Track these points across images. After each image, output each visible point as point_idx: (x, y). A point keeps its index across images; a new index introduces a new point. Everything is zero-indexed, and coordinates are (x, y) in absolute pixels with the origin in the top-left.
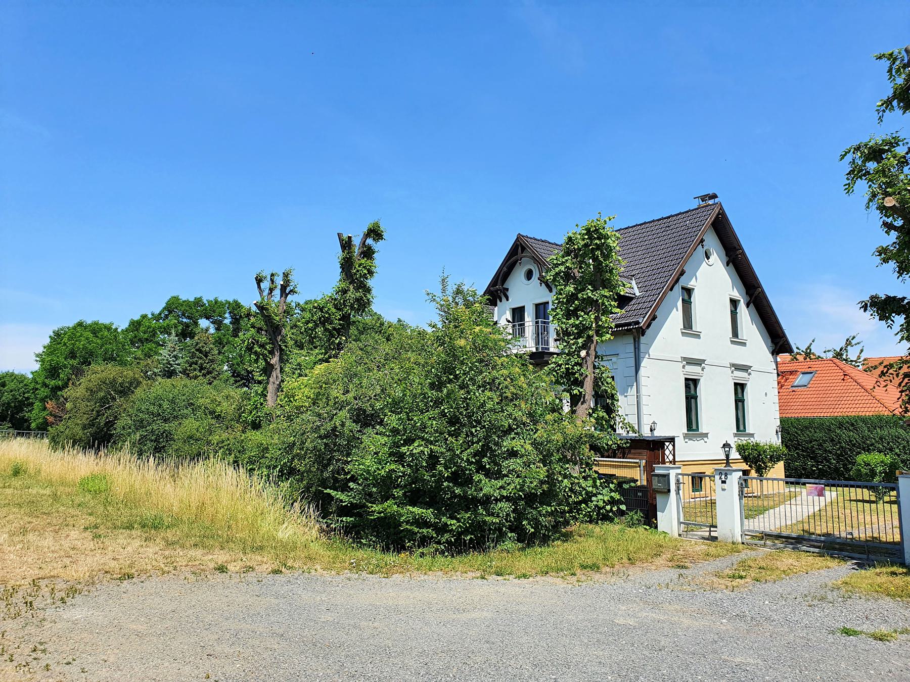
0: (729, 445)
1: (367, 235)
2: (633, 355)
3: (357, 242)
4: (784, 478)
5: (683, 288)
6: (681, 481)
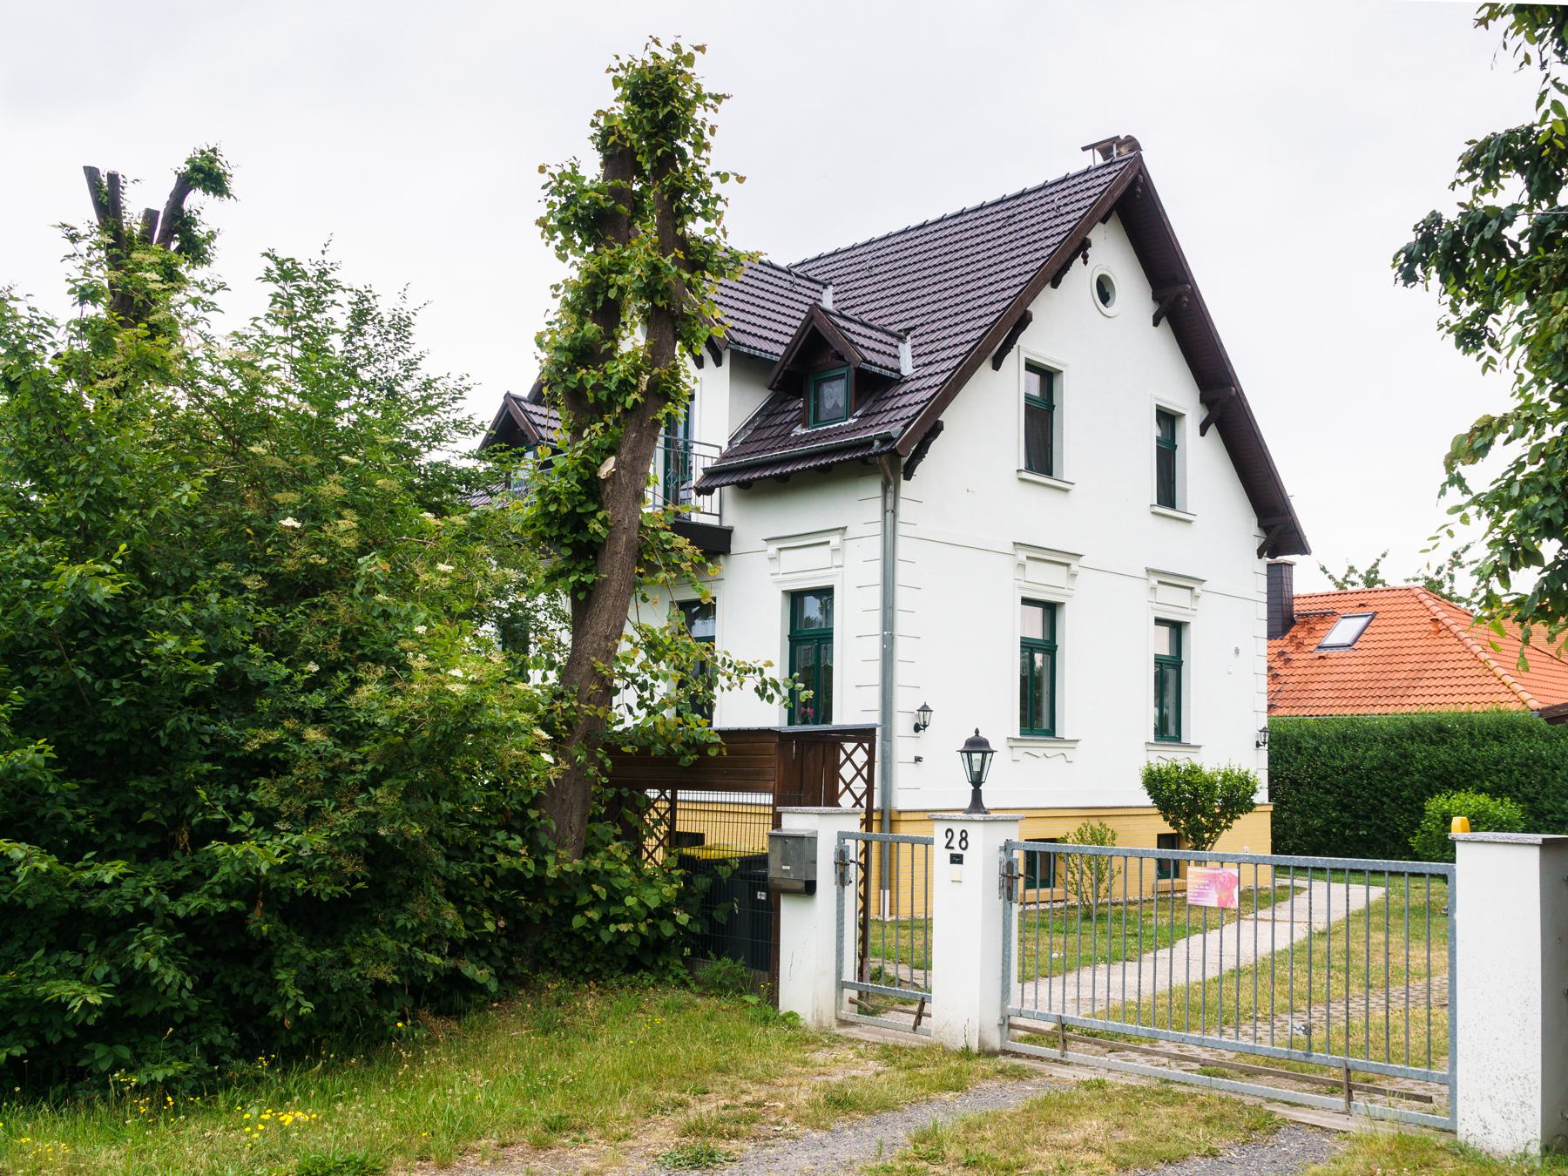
0: (985, 743)
1: (185, 184)
2: (878, 529)
4: (1269, 854)
5: (1031, 367)
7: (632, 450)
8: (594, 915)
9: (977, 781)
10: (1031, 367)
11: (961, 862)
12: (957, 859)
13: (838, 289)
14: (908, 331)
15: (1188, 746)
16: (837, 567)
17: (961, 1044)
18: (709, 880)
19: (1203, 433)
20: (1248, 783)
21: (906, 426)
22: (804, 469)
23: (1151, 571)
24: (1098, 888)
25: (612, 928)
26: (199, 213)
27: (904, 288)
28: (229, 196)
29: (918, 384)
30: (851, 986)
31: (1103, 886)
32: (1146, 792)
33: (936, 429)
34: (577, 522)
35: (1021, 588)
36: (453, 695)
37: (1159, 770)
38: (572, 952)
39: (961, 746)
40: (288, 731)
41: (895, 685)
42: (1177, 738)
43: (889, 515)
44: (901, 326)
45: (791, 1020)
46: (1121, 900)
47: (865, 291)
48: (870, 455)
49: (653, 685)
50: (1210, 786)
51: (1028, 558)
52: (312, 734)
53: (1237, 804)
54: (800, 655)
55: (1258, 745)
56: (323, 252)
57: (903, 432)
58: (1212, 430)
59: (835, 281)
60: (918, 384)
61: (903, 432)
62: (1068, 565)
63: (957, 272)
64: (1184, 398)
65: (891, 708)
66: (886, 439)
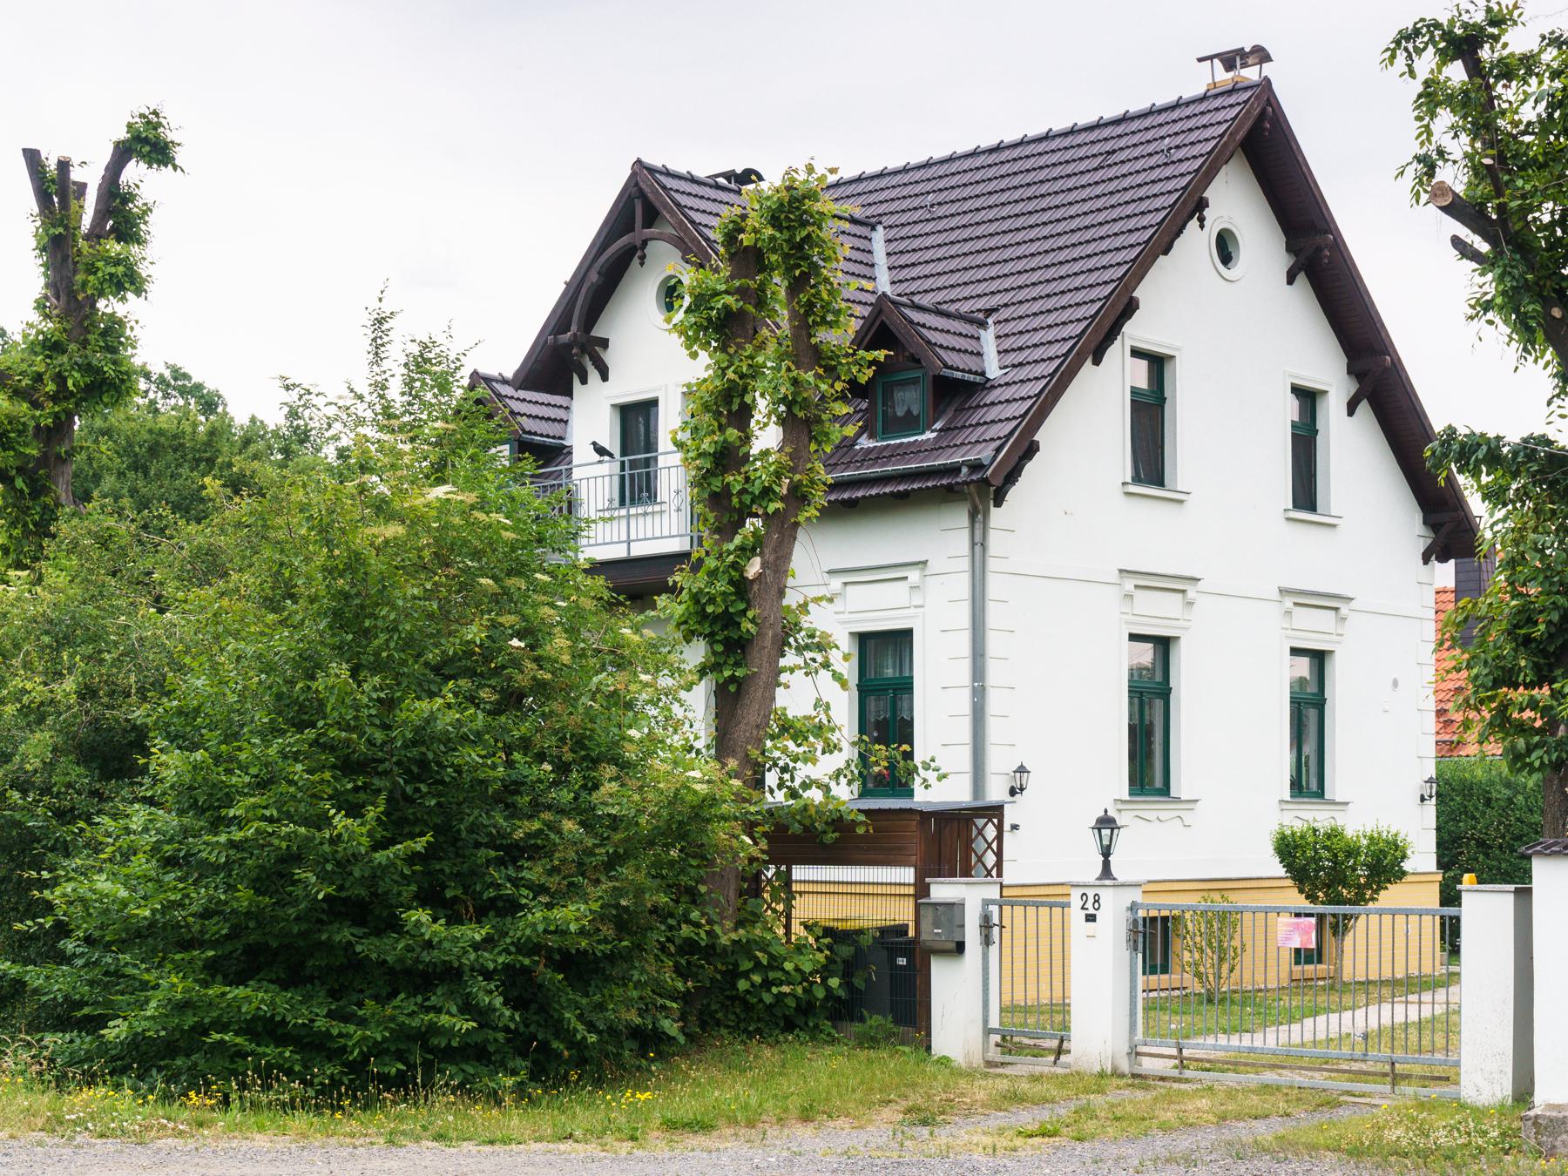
0: (1113, 821)
1: (123, 153)
2: (965, 564)
3: (90, 175)
5: (1136, 353)
6: (996, 920)
7: (775, 550)
8: (757, 979)
9: (1106, 853)
10: (1136, 353)
11: (1094, 920)
12: (1091, 918)
13: (892, 233)
14: (989, 312)
15: (1333, 803)
16: (916, 607)
17: (1097, 1069)
18: (852, 949)
19: (1351, 412)
20: (1397, 847)
21: (998, 450)
22: (878, 495)
23: (1283, 591)
24: (1220, 968)
25: (774, 990)
26: (137, 186)
27: (979, 245)
28: (175, 168)
29: (1008, 393)
30: (995, 1031)
31: (1225, 968)
32: (1278, 860)
33: (1031, 450)
34: (728, 620)
35: (1127, 623)
36: (695, 792)
37: (1293, 834)
38: (735, 1013)
39: (1093, 823)
40: (545, 823)
41: (988, 744)
42: (1320, 793)
43: (978, 548)
44: (982, 303)
45: (944, 1061)
46: (1250, 988)
47: (929, 241)
48: (957, 483)
49: (794, 768)
50: (1352, 852)
51: (1137, 587)
52: (568, 825)
53: (1384, 872)
54: (872, 704)
55: (1423, 799)
56: (380, 300)
57: (995, 457)
58: (1364, 408)
59: (887, 220)
60: (1008, 393)
61: (995, 457)
62: (1183, 591)
63: (1064, 300)
64: (1327, 371)
65: (983, 770)
66: (976, 466)
